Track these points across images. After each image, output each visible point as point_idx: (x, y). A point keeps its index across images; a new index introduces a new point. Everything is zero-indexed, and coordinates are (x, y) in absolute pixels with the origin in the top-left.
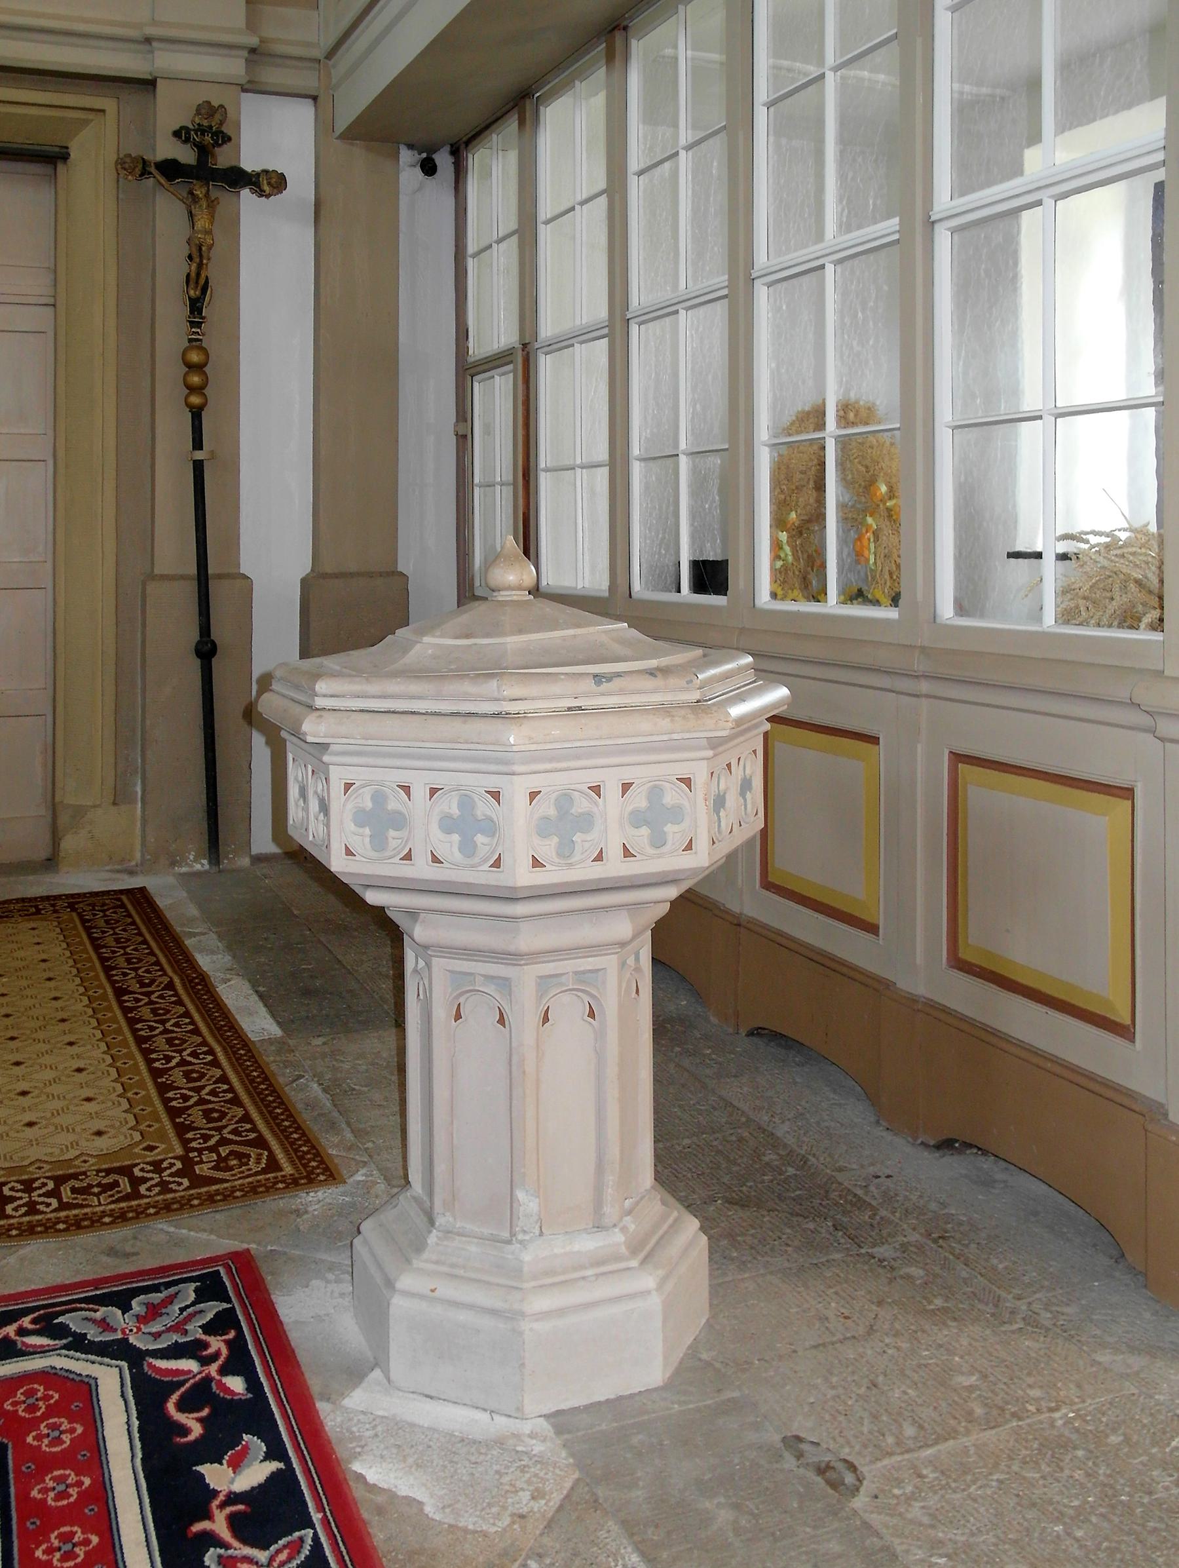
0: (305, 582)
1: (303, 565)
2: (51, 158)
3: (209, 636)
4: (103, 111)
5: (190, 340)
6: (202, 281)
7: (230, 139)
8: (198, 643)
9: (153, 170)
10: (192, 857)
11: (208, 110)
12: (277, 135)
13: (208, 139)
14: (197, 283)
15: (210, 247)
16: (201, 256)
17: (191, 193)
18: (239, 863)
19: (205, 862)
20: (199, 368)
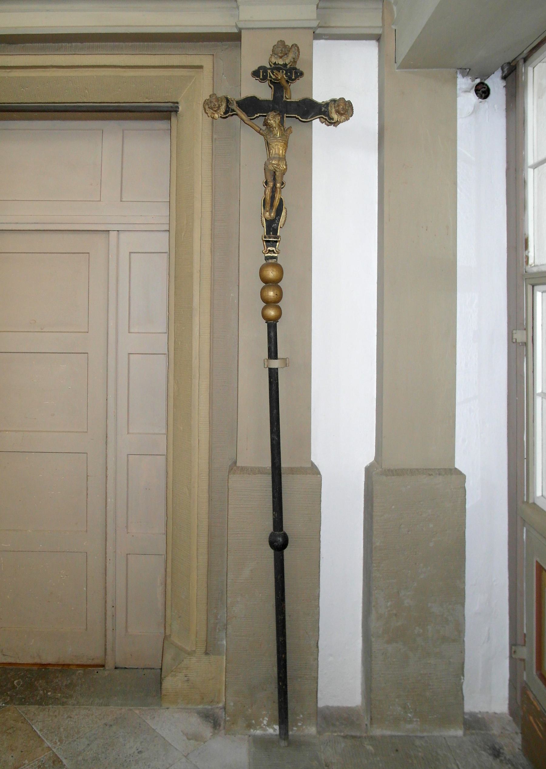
0: (368, 470)
1: (368, 455)
2: (165, 112)
3: (281, 529)
4: (201, 67)
5: (267, 258)
6: (276, 203)
7: (302, 74)
8: (271, 535)
9: (235, 107)
10: (265, 722)
11: (282, 49)
12: (344, 70)
13: (281, 76)
14: (272, 205)
15: (283, 173)
16: (274, 179)
17: (266, 124)
18: (306, 731)
19: (277, 727)
20: (273, 284)
